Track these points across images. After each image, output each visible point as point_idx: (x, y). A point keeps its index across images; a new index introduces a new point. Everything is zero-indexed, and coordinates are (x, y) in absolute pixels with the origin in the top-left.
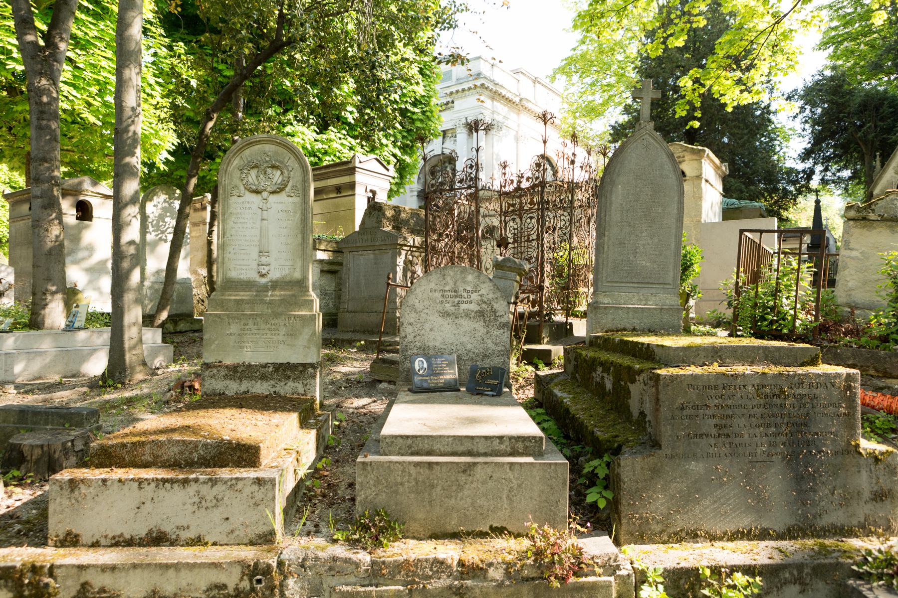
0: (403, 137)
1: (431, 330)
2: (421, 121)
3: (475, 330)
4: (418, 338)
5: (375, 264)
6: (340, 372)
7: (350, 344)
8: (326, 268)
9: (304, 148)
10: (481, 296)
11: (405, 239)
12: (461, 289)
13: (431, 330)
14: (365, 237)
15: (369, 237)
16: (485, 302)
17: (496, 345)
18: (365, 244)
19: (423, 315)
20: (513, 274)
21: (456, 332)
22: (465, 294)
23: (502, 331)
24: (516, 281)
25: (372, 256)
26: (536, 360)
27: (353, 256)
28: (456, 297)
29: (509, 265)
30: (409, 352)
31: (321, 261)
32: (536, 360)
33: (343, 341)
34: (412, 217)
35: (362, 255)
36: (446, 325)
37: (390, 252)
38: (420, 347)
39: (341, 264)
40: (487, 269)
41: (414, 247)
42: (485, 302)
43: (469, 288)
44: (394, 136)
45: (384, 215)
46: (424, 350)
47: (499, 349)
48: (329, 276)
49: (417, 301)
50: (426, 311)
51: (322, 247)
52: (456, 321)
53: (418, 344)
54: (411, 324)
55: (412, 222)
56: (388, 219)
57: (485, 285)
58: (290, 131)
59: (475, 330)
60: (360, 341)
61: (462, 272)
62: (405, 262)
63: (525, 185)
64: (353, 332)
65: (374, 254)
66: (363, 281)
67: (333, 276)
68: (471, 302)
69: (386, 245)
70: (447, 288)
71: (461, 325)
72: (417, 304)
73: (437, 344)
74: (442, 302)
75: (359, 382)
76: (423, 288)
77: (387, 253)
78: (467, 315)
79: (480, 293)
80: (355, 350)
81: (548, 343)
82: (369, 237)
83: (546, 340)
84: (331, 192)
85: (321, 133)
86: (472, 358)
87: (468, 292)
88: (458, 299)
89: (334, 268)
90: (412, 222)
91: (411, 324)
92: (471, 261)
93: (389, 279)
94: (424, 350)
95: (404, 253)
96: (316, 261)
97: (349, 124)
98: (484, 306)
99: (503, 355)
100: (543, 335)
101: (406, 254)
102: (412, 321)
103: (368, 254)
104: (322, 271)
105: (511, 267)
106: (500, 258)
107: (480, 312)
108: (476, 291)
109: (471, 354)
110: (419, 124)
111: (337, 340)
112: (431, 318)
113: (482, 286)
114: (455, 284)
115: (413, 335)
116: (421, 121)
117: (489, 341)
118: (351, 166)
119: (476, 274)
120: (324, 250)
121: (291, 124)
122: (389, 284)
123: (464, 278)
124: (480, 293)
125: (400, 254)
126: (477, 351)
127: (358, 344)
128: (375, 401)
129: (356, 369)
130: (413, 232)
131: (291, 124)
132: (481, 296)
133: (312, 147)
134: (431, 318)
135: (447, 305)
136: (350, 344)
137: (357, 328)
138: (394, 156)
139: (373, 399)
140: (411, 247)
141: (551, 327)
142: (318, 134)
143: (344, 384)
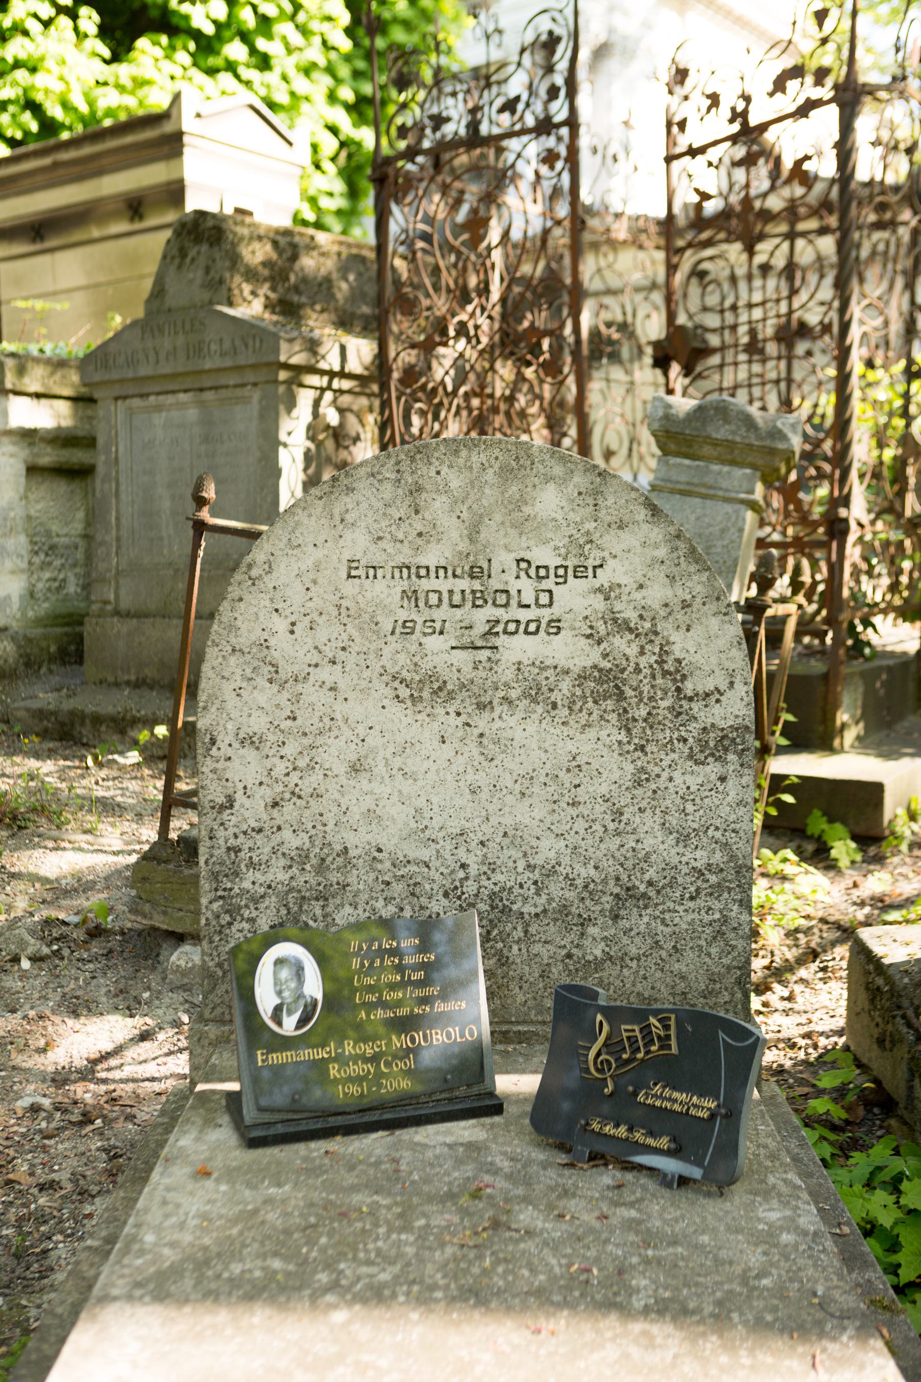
0: (357, 74)
1: (355, 769)
2: (407, 25)
3: (575, 766)
4: (289, 812)
5: (206, 439)
6: (34, 878)
7: (123, 732)
8: (48, 457)
9: (66, 105)
10: (606, 593)
11: (313, 346)
12: (504, 559)
13: (355, 769)
14: (166, 343)
15: (181, 340)
16: (625, 627)
17: (683, 839)
18: (166, 369)
19: (311, 693)
20: (740, 473)
21: (481, 779)
22: (527, 588)
23: (713, 769)
24: (753, 506)
25: (192, 414)
26: (817, 823)
27: (131, 413)
28: (478, 600)
29: (721, 432)
30: (249, 881)
31: (28, 435)
32: (817, 823)
33: (97, 720)
34: (344, 269)
35: (159, 408)
36: (430, 743)
37: (256, 395)
38: (303, 857)
39: (90, 442)
40: (608, 454)
41: (342, 374)
42: (625, 627)
43: (544, 556)
44: (330, 70)
45: (235, 259)
46: (322, 867)
47: (701, 858)
48: (62, 486)
49: (280, 625)
50: (326, 674)
51: (33, 384)
52: (482, 722)
53: (292, 841)
54: (251, 741)
55: (343, 289)
56: (251, 275)
57: (629, 539)
58: (22, 56)
59: (575, 766)
60: (152, 723)
61: (506, 473)
62: (312, 432)
63: (711, 207)
64: (138, 684)
65: (201, 404)
66: (167, 504)
67: (76, 485)
68: (555, 627)
69: (238, 368)
70: (431, 557)
71: (504, 744)
72: (282, 644)
73: (389, 838)
74: (408, 628)
75: (96, 932)
76: (312, 556)
77: (246, 400)
78: (534, 694)
79: (604, 578)
80: (134, 757)
81: (864, 743)
82: (181, 340)
83: (850, 736)
84: (113, 216)
85: (116, 58)
86: (564, 909)
87: (541, 573)
88: (490, 612)
89: (77, 456)
90: (343, 289)
91: (251, 741)
92: (554, 425)
93: (201, 502)
94: (322, 867)
95: (305, 398)
96: (9, 433)
97: (197, 35)
98: (622, 645)
99: (717, 890)
100: (843, 717)
101: (317, 403)
102: (257, 724)
103: (181, 406)
104: (32, 470)
105: (729, 445)
106: (683, 404)
107: (602, 676)
108: (579, 572)
109: (556, 889)
110: (398, 35)
111: (76, 717)
112: (354, 710)
113: (613, 542)
114: (473, 533)
115: (267, 794)
116: (407, 25)
117: (649, 822)
118: (168, 128)
119: (580, 480)
120: (38, 396)
121: (26, 33)
122: (200, 527)
123: (522, 501)
124: (604, 578)
125: (291, 404)
126: (586, 872)
127: (144, 736)
128: (145, 1036)
129: (102, 862)
130: (345, 322)
131: (26, 33)
132: (606, 593)
133: (91, 104)
134: (354, 710)
135: (434, 643)
136: (123, 732)
137: (149, 673)
138: (333, 130)
139: (139, 1023)
140: (332, 374)
141: (868, 677)
142: (106, 62)
143: (34, 945)
